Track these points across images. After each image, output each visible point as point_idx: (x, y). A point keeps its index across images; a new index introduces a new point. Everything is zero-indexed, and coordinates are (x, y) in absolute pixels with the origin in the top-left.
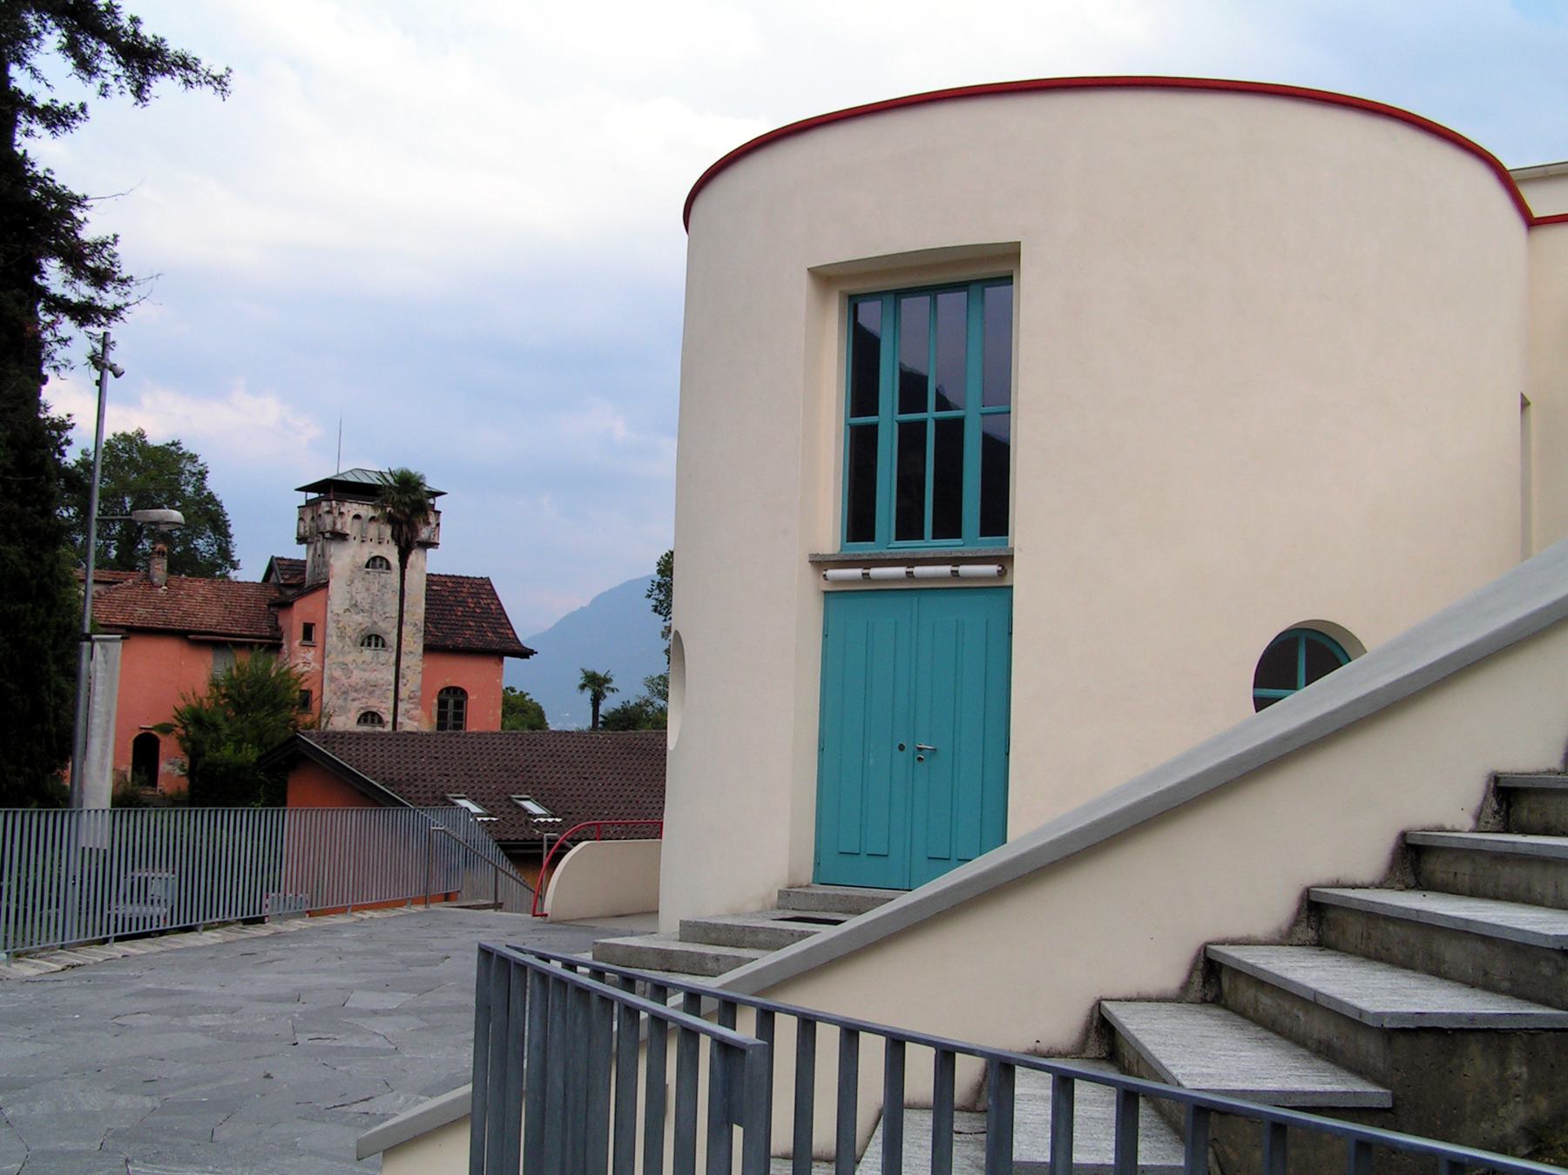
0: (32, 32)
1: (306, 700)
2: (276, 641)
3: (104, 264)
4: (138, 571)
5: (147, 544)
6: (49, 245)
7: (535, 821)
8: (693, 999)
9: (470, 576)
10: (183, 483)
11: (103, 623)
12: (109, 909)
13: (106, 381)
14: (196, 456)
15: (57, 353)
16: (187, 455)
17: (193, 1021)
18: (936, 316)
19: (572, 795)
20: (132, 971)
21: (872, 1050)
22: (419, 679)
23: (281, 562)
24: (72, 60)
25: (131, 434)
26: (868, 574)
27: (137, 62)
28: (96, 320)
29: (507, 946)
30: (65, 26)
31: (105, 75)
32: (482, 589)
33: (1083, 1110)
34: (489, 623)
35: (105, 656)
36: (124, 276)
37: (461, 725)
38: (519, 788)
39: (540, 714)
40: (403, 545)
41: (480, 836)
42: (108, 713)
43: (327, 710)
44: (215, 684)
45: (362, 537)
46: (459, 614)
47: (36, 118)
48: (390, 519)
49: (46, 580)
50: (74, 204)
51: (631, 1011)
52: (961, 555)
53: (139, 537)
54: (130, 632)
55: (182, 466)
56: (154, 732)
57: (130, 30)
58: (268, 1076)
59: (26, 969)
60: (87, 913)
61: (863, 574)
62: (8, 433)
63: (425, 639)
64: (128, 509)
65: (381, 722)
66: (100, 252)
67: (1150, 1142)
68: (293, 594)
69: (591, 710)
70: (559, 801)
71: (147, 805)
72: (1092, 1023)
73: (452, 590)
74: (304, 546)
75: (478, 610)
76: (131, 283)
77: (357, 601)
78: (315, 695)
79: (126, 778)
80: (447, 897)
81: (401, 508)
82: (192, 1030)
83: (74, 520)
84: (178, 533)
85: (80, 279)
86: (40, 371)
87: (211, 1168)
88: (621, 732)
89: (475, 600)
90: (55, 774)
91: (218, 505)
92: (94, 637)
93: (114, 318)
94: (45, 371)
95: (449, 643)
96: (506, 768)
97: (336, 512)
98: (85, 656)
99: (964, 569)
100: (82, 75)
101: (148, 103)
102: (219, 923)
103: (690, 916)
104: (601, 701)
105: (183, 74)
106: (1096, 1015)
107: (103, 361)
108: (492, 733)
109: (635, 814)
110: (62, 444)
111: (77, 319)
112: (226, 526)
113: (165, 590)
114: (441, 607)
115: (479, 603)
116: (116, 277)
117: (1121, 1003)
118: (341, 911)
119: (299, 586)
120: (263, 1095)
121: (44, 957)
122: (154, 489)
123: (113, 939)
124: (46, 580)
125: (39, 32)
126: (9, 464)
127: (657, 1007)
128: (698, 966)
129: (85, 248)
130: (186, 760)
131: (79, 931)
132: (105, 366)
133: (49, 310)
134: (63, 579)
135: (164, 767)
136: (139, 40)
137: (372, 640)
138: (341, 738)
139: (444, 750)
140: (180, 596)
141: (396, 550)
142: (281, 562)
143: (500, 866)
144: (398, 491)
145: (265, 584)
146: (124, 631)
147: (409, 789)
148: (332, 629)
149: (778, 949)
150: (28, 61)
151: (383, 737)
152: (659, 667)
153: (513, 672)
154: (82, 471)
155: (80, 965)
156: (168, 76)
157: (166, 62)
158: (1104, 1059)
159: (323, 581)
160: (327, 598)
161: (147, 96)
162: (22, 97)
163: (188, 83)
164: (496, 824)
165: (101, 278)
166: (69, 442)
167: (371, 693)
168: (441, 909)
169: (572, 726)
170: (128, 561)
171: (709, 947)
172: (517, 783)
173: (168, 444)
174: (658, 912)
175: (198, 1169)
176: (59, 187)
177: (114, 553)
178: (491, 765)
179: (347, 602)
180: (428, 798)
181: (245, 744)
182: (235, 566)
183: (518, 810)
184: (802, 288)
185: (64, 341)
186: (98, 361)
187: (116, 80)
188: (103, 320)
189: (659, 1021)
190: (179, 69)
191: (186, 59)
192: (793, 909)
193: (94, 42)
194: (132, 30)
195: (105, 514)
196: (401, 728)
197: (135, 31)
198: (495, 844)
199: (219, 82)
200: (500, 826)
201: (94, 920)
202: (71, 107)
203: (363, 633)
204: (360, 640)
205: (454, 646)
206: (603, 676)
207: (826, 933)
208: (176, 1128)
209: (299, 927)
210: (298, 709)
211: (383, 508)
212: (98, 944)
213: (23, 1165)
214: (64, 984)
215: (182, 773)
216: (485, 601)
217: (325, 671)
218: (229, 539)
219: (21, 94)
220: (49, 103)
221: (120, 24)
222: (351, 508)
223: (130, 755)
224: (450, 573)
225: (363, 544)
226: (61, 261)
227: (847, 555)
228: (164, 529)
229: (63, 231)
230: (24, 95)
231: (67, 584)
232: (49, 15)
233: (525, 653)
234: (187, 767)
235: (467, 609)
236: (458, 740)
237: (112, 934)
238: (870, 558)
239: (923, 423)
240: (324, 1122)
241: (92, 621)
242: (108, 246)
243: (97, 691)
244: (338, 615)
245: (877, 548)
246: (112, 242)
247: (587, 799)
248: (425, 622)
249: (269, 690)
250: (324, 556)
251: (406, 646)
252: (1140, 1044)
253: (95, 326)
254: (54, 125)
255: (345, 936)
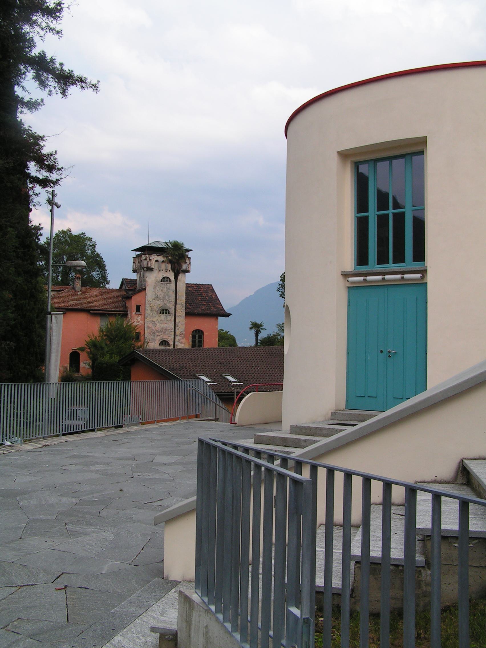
0: (22, 72)
1: (138, 336)
2: (125, 313)
3: (52, 162)
4: (70, 286)
5: (73, 275)
6: (31, 157)
7: (232, 384)
8: (284, 461)
9: (204, 284)
10: (86, 249)
11: (56, 307)
12: (62, 422)
13: (54, 209)
14: (92, 239)
15: (35, 199)
16: (88, 238)
17: (92, 468)
18: (392, 170)
19: (247, 373)
20: (69, 448)
21: (357, 483)
22: (184, 327)
23: (126, 280)
24: (38, 82)
25: (65, 230)
26: (403, 277)
27: (62, 81)
28: (49, 185)
29: (210, 439)
30: (35, 69)
31: (50, 87)
32: (209, 289)
33: (454, 506)
34: (212, 303)
35: (56, 321)
36: (60, 167)
37: (201, 345)
38: (225, 371)
39: (234, 340)
40: (176, 272)
41: (209, 390)
42: (58, 343)
43: (147, 340)
44: (101, 331)
45: (159, 269)
46: (200, 299)
47: (24, 106)
48: (170, 262)
49: (33, 290)
50: (39, 139)
51: (258, 466)
52: (405, 270)
53: (70, 272)
54: (66, 311)
55: (86, 243)
56: (78, 351)
57: (60, 68)
58: (121, 490)
59: (28, 447)
60: (54, 424)
61: (364, 279)
62: (16, 233)
63: (186, 310)
64: (65, 261)
65: (169, 344)
66: (50, 158)
67: (483, 521)
68: (132, 293)
69: (255, 338)
70: (242, 376)
71: (75, 380)
72: (459, 468)
73: (196, 290)
74: (136, 273)
75: (207, 298)
76: (63, 170)
77: (157, 296)
78: (142, 334)
79: (67, 369)
80: (197, 416)
81: (174, 257)
82: (92, 472)
83: (44, 266)
84: (85, 270)
85: (43, 169)
86: (29, 207)
87: (98, 527)
88: (267, 347)
89: (206, 294)
90: (39, 368)
91: (101, 258)
92: (52, 313)
93: (56, 184)
94: (31, 207)
95: (195, 311)
96: (220, 363)
97: (148, 259)
98: (49, 321)
99: (406, 276)
100: (41, 88)
101: (67, 97)
102: (105, 427)
103: (294, 423)
104: (259, 334)
105: (81, 84)
106: (461, 466)
107: (52, 202)
108: (214, 348)
109: (274, 381)
110: (39, 236)
111: (42, 185)
112: (104, 266)
113: (80, 293)
114: (192, 297)
115: (208, 295)
116: (56, 167)
117: (472, 460)
118: (152, 422)
119: (134, 290)
120: (119, 498)
121: (35, 442)
122: (75, 252)
123: (61, 435)
124: (33, 290)
125: (25, 72)
126: (17, 245)
127: (269, 465)
128: (298, 444)
129: (44, 157)
130: (91, 362)
131: (48, 432)
132: (53, 204)
133: (31, 182)
134: (40, 290)
135: (82, 365)
136: (63, 72)
137: (164, 311)
138: (152, 352)
139: (194, 356)
140: (86, 295)
141: (173, 274)
142: (126, 280)
143: (217, 403)
144: (173, 250)
145: (121, 290)
146: (65, 310)
147: (180, 372)
148: (148, 307)
149: (329, 437)
150: (21, 84)
151: (169, 351)
152: (282, 319)
153: (222, 323)
154: (47, 246)
155: (49, 445)
156: (75, 86)
157: (74, 80)
158: (465, 484)
159: (144, 288)
160: (146, 294)
161: (67, 94)
162: (19, 98)
163: (82, 88)
164: (216, 386)
165: (51, 168)
166: (41, 235)
167: (164, 333)
168: (193, 421)
169: (247, 345)
170: (65, 282)
171: (302, 436)
172: (225, 368)
173: (80, 234)
174: (281, 421)
175: (93, 528)
176: (33, 133)
177: (60, 279)
178: (214, 362)
179: (154, 296)
180: (188, 375)
181: (114, 355)
182: (108, 283)
183: (225, 380)
184: (334, 161)
185: (37, 195)
186: (51, 202)
187: (54, 89)
188: (52, 185)
189: (269, 470)
190: (79, 82)
191: (81, 78)
192: (337, 420)
193: (46, 74)
194: (60, 68)
195: (56, 263)
196: (177, 347)
197: (61, 69)
198: (215, 394)
199: (95, 87)
200: (218, 386)
201: (57, 427)
202: (38, 101)
203: (160, 308)
204: (159, 312)
205: (198, 313)
206: (259, 324)
207: (350, 429)
208: (85, 511)
209: (136, 429)
210: (135, 340)
211: (167, 257)
212: (56, 437)
213: (27, 524)
214: (42, 453)
215: (89, 367)
216: (210, 294)
217: (146, 324)
218: (105, 272)
219: (19, 97)
220: (29, 100)
221: (56, 66)
222: (154, 257)
223: (69, 360)
224: (195, 283)
225: (160, 272)
226: (35, 162)
227: (357, 271)
228: (80, 268)
229: (35, 150)
230: (20, 97)
231: (42, 292)
232: (29, 65)
233: (227, 315)
234: (91, 365)
235: (203, 298)
236: (200, 351)
237: (61, 433)
238: (366, 272)
239: (387, 215)
240: (144, 509)
241: (51, 306)
242: (53, 155)
243: (54, 335)
244: (150, 301)
245: (370, 268)
246: (55, 154)
247: (253, 375)
248: (186, 303)
249: (122, 333)
250: (144, 278)
251: (178, 313)
252: (479, 478)
253: (49, 188)
254: (31, 108)
255: (154, 433)
